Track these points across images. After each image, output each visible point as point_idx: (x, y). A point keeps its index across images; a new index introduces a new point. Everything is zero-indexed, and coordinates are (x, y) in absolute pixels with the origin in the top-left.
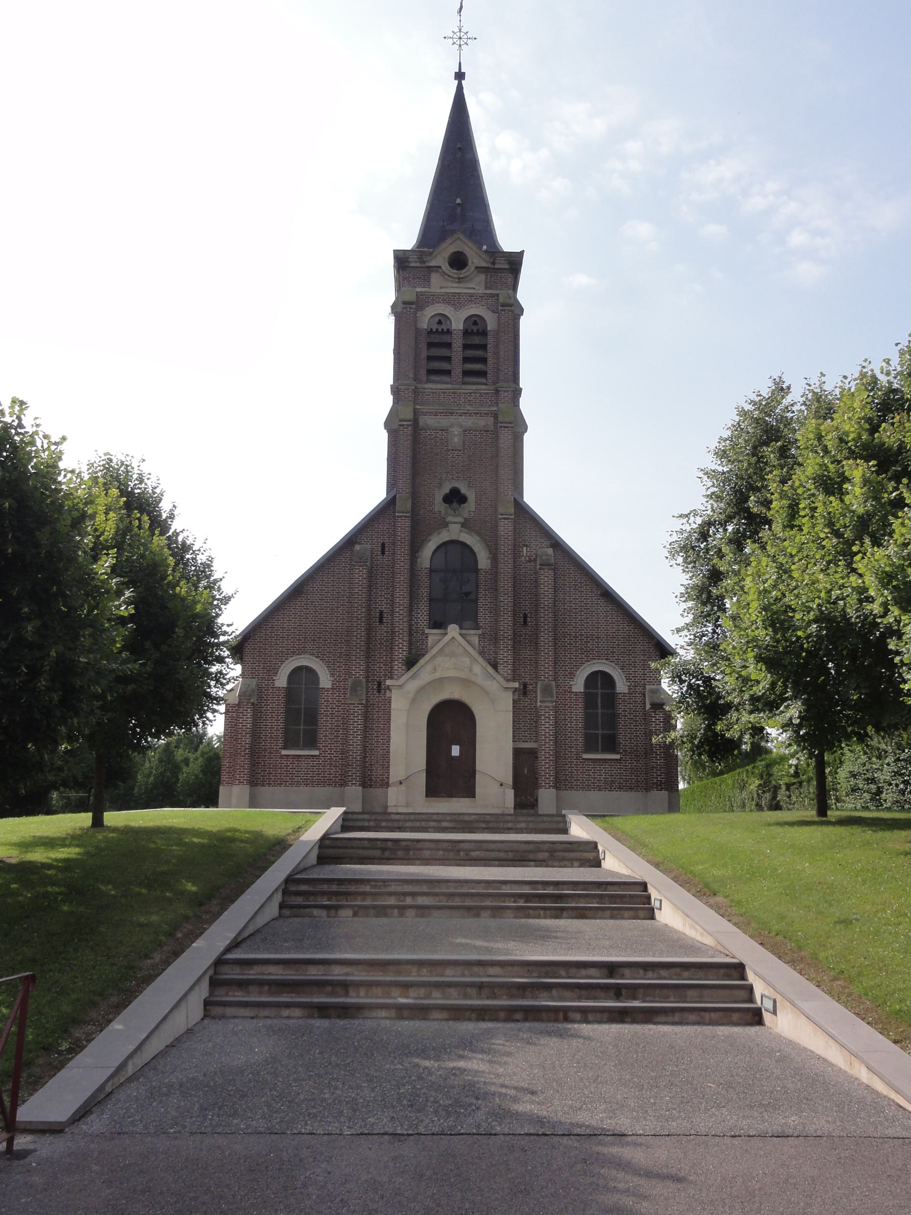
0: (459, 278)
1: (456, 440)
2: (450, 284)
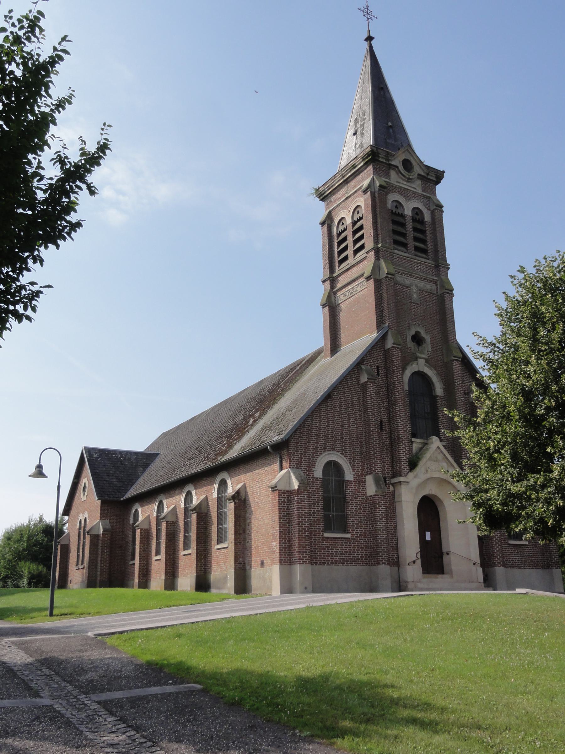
0: (409, 179)
1: (415, 296)
2: (402, 181)
